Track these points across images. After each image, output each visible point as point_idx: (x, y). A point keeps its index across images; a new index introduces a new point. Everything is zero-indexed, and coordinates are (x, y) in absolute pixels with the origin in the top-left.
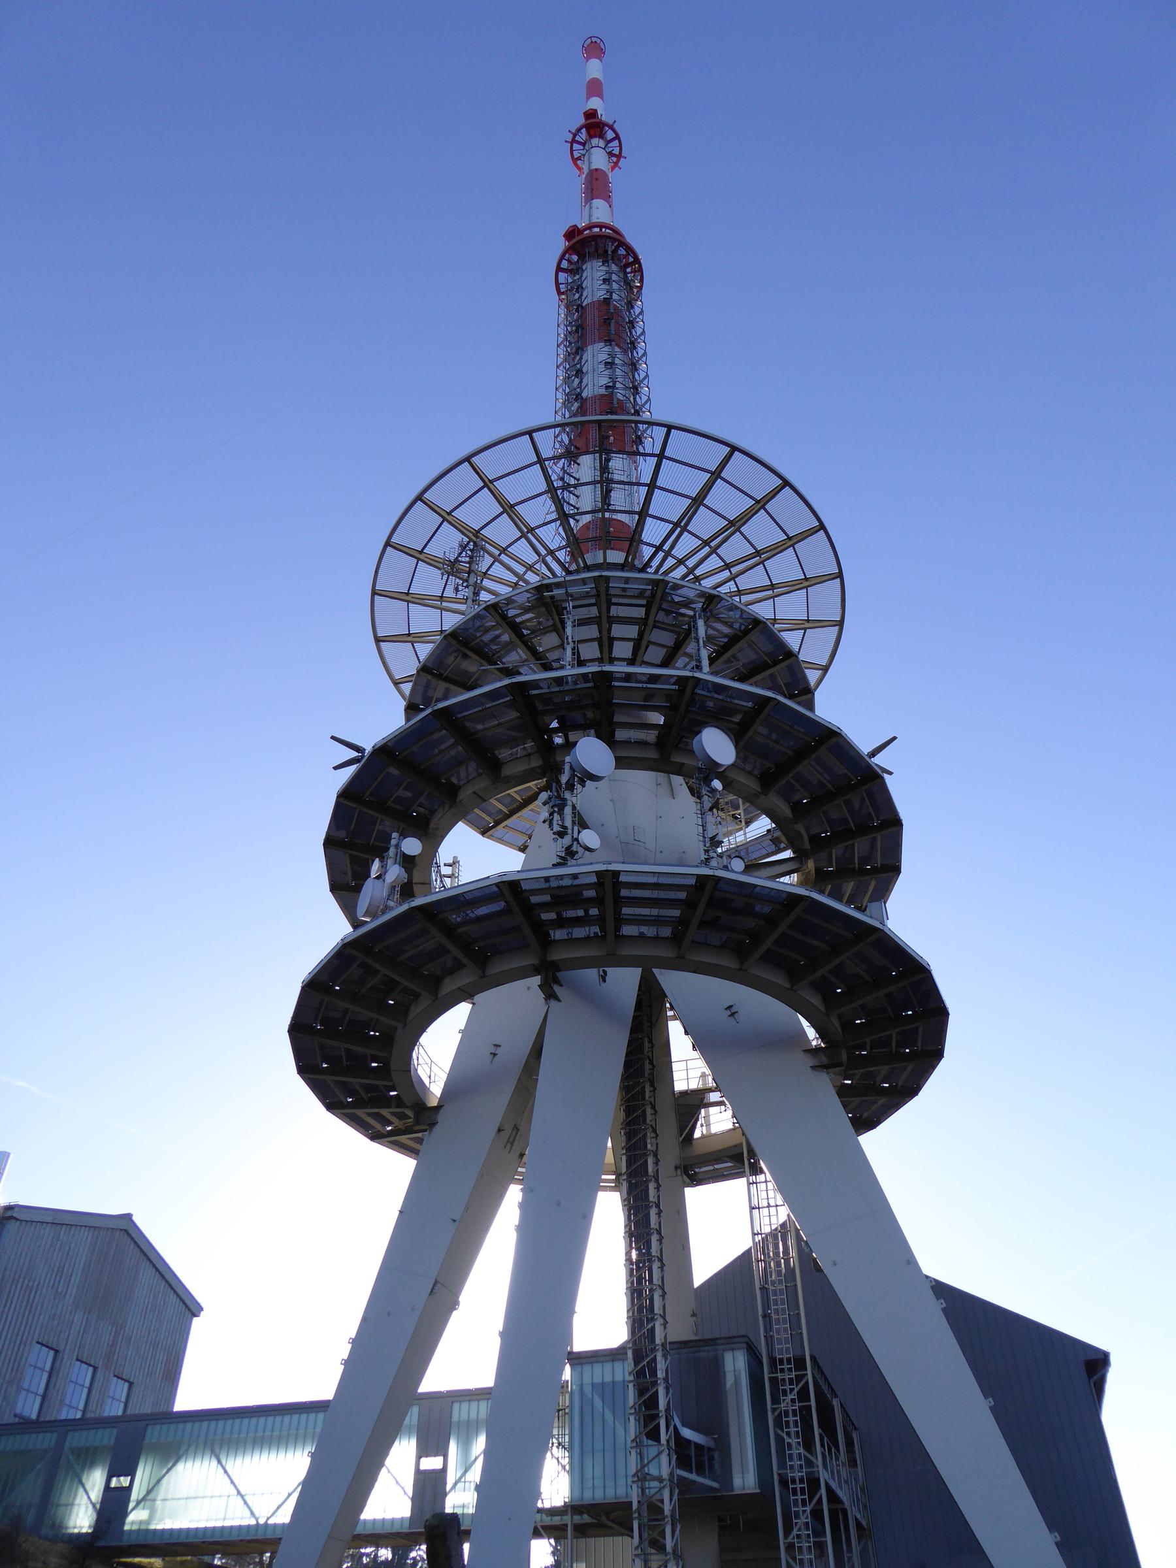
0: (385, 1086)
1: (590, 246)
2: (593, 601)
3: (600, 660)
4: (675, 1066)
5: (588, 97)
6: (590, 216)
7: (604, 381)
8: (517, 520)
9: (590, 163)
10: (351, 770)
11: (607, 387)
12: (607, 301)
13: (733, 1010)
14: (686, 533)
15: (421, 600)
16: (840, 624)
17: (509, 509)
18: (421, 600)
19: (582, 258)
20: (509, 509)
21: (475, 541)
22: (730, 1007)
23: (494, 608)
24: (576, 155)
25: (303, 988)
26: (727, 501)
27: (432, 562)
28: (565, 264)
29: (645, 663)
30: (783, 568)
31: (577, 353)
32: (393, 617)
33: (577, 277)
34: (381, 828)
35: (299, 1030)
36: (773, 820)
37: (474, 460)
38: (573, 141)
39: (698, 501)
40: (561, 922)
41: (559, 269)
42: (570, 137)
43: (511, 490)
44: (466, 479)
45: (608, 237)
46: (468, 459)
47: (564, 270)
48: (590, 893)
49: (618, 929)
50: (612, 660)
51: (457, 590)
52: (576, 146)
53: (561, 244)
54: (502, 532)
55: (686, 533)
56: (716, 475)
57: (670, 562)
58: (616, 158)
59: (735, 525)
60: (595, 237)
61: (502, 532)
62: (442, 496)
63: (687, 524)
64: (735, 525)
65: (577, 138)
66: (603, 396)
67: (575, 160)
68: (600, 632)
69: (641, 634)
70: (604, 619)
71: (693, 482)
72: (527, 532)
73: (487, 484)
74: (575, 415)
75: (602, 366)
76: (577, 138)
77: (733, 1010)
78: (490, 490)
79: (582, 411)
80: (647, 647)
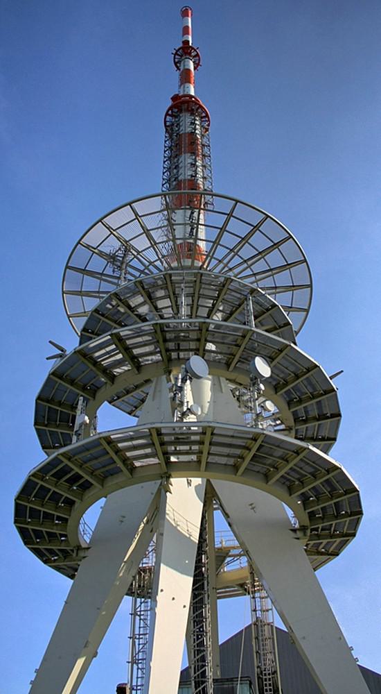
0: (60, 534)
1: (182, 105)
2: (192, 285)
4: (216, 534)
5: (183, 36)
6: (184, 91)
7: (190, 173)
8: (150, 237)
9: (184, 66)
10: (58, 362)
11: (192, 176)
13: (253, 506)
14: (236, 256)
15: (92, 274)
16: (307, 311)
17: (147, 232)
18: (92, 274)
19: (180, 111)
20: (147, 232)
21: (127, 247)
22: (251, 505)
24: (176, 60)
27: (101, 254)
28: (170, 112)
30: (283, 279)
31: (176, 157)
32: (74, 280)
33: (177, 120)
37: (133, 205)
38: (176, 54)
40: (176, 453)
41: (167, 114)
42: (174, 52)
43: (150, 223)
45: (193, 102)
46: (130, 204)
47: (170, 115)
48: (197, 438)
51: (114, 271)
52: (177, 57)
53: (170, 103)
54: (141, 243)
55: (236, 256)
57: (248, 272)
58: (197, 66)
60: (187, 102)
61: (141, 243)
63: (238, 251)
64: (262, 254)
65: (178, 53)
66: (189, 180)
67: (176, 63)
68: (193, 301)
69: (214, 305)
70: (196, 295)
71: (244, 230)
72: (154, 244)
74: (174, 189)
75: (189, 165)
76: (178, 53)
77: (253, 506)
78: (138, 220)
79: (179, 186)
80: (197, 308)
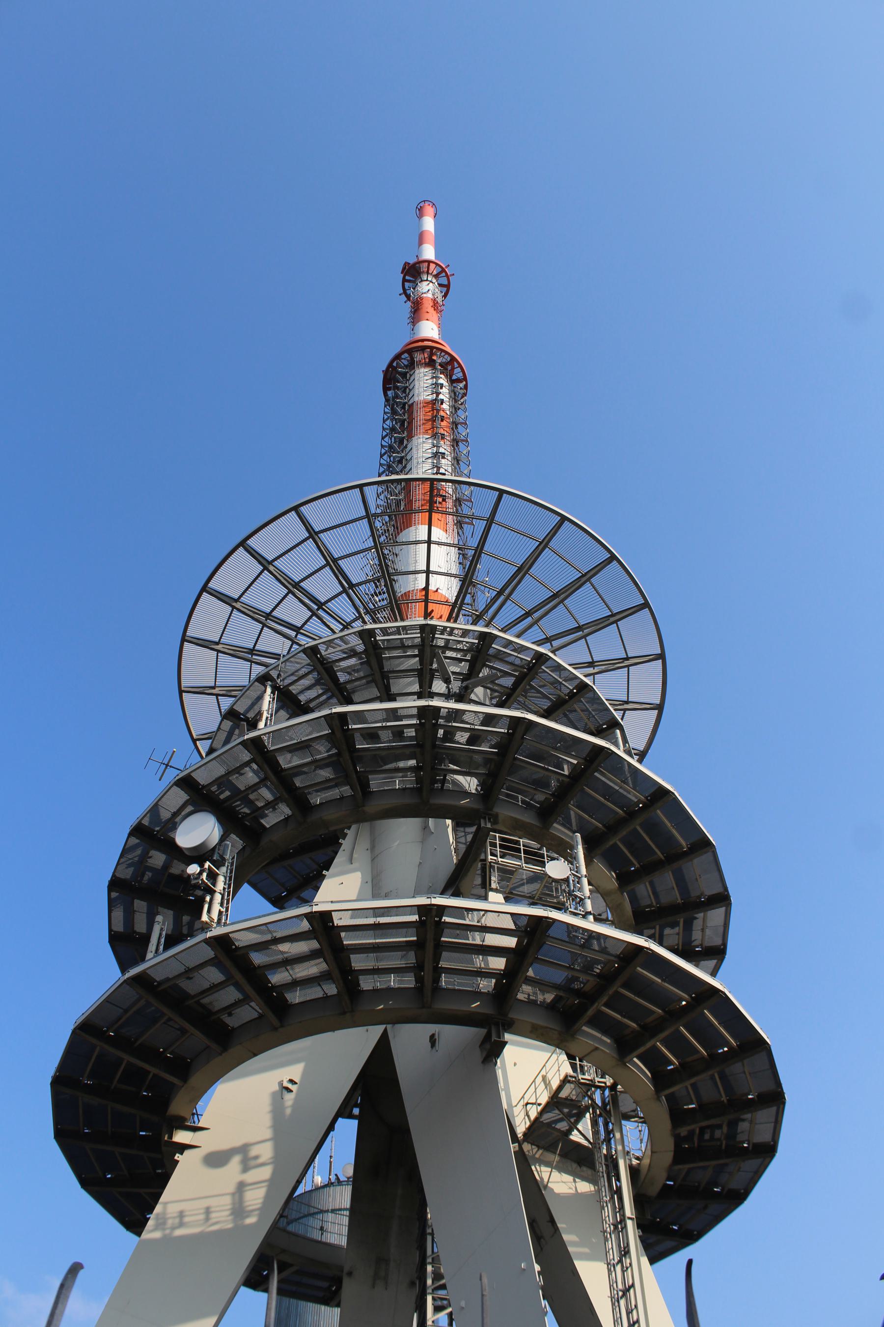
3: (420, 696)
8: (340, 573)
12: (433, 402)
17: (333, 563)
23: (312, 652)
25: (74, 1032)
26: (552, 572)
29: (471, 701)
30: (604, 645)
34: (676, 930)
35: (63, 1083)
36: (133, 903)
39: (523, 570)
42: (404, 298)
44: (289, 529)
49: (437, 958)
50: (432, 695)
56: (544, 544)
59: (558, 597)
62: (267, 543)
64: (558, 597)
73: (313, 534)
